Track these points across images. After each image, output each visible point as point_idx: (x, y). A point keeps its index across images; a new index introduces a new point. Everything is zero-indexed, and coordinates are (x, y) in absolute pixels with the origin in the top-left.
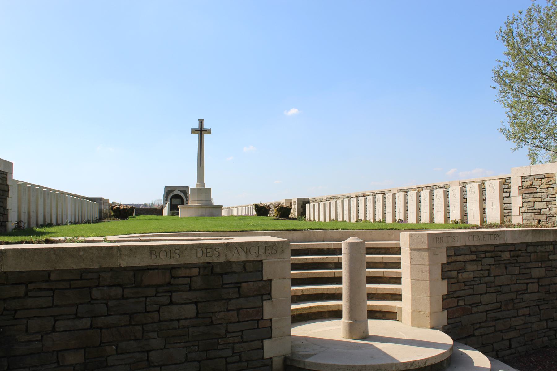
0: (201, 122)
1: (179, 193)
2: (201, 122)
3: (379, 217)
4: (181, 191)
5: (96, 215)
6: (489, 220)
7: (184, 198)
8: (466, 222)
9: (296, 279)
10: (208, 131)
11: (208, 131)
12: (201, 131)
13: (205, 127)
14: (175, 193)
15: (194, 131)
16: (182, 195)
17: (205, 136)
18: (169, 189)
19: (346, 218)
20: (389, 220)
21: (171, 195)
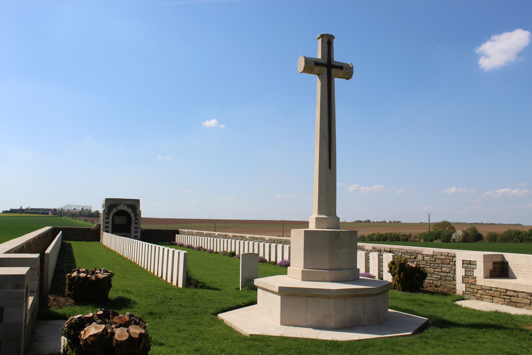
0: (328, 41)
1: (125, 208)
2: (328, 41)
3: (200, 245)
4: (129, 206)
5: (389, 250)
6: (272, 260)
7: (132, 215)
8: (382, 279)
9: (281, 318)
10: (347, 72)
11: (347, 72)
12: (328, 69)
13: (338, 57)
14: (120, 208)
15: (311, 66)
16: (129, 211)
17: (339, 83)
18: (112, 203)
19: (225, 250)
20: (279, 260)
21: (115, 210)
